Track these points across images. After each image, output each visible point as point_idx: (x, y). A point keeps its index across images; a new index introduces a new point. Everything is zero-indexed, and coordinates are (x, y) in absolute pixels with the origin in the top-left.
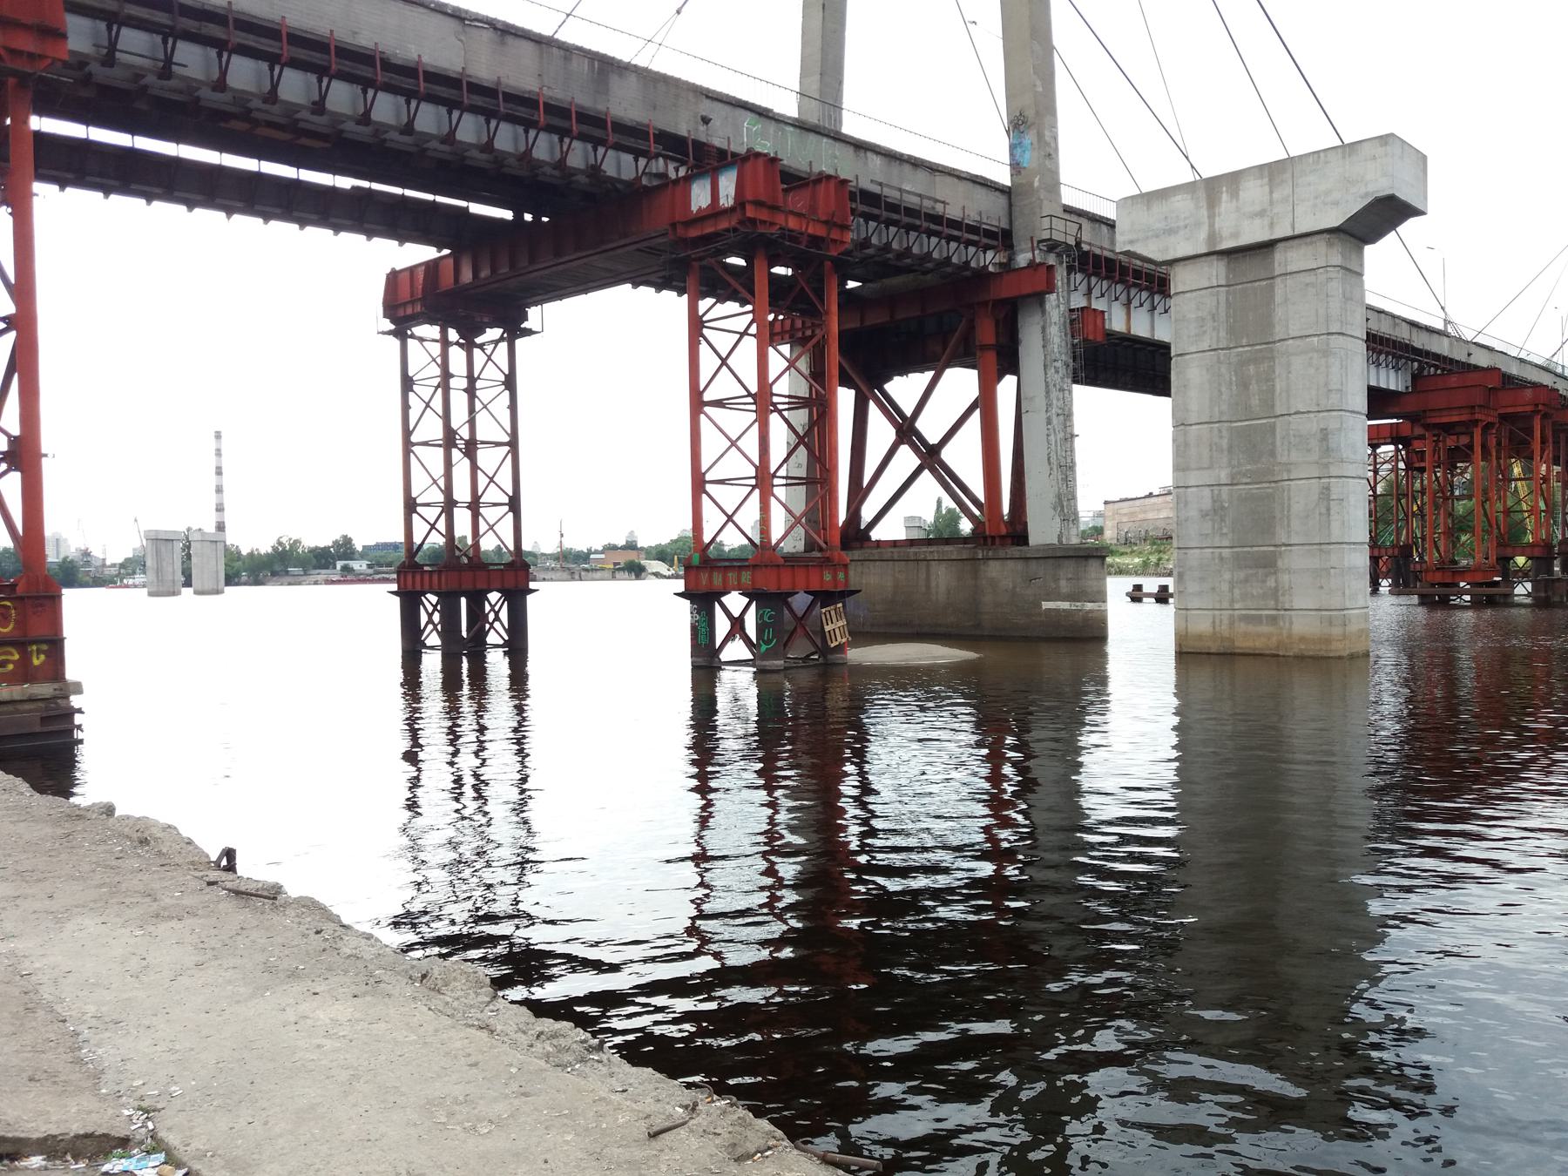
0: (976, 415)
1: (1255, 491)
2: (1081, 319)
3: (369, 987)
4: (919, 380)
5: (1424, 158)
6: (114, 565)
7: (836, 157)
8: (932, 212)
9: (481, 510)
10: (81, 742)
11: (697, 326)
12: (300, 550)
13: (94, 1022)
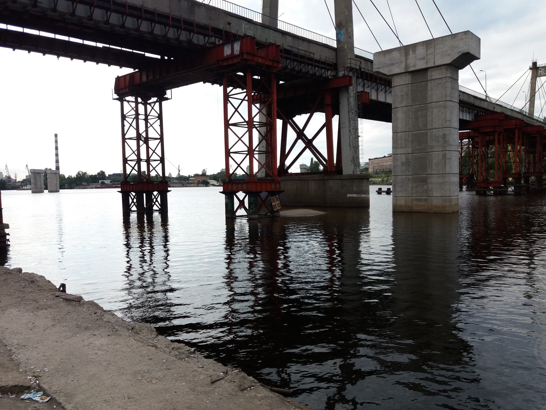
0: (324, 130)
1: (420, 156)
2: (361, 96)
3: (114, 333)
4: (305, 116)
5: (480, 39)
6: (19, 182)
7: (275, 37)
8: (309, 57)
9: (151, 162)
10: (9, 245)
11: (226, 97)
12: (86, 176)
13: (17, 346)
